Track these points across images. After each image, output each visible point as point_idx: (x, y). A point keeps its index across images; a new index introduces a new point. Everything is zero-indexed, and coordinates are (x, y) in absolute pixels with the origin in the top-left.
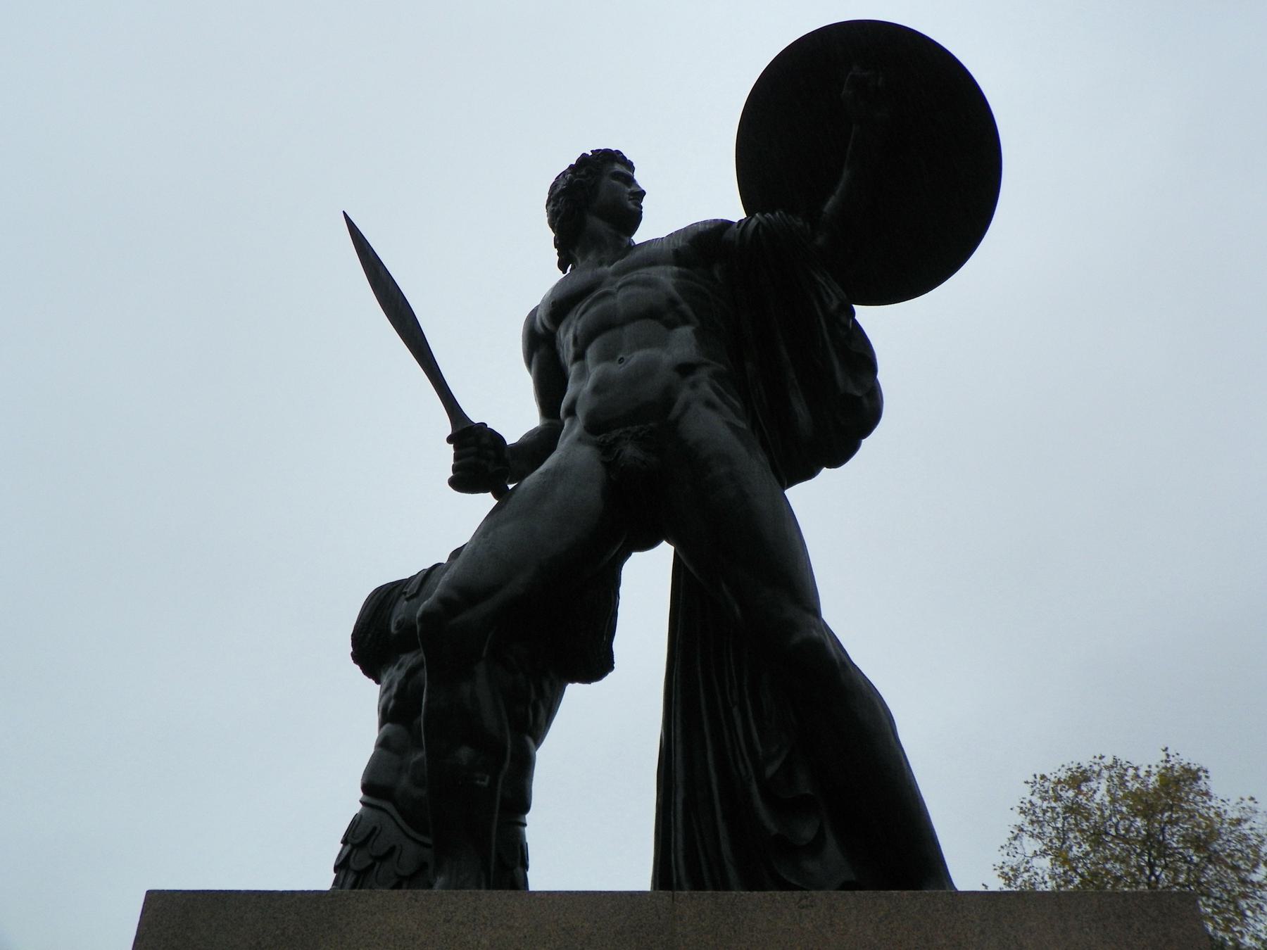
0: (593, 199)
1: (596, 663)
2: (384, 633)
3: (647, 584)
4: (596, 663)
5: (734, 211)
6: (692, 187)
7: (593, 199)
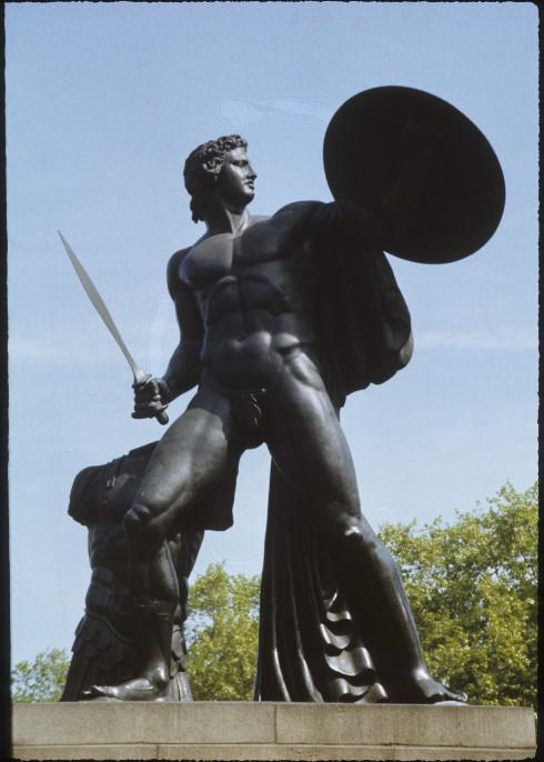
0: (213, 183)
1: (224, 522)
4: (224, 522)
6: (288, 175)
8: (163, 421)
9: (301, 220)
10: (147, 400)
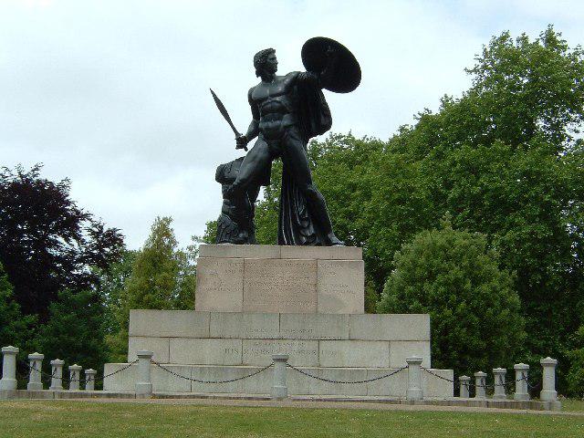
0: (265, 63)
2: (223, 175)
3: (277, 164)
5: (303, 70)
6: (290, 64)
7: (265, 63)
8: (246, 150)
9: (296, 79)
10: (242, 142)
